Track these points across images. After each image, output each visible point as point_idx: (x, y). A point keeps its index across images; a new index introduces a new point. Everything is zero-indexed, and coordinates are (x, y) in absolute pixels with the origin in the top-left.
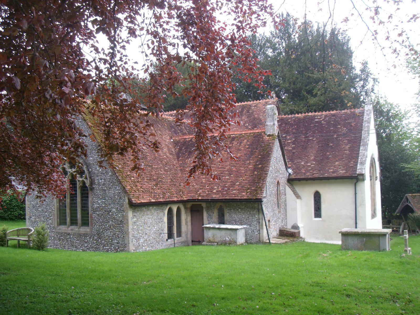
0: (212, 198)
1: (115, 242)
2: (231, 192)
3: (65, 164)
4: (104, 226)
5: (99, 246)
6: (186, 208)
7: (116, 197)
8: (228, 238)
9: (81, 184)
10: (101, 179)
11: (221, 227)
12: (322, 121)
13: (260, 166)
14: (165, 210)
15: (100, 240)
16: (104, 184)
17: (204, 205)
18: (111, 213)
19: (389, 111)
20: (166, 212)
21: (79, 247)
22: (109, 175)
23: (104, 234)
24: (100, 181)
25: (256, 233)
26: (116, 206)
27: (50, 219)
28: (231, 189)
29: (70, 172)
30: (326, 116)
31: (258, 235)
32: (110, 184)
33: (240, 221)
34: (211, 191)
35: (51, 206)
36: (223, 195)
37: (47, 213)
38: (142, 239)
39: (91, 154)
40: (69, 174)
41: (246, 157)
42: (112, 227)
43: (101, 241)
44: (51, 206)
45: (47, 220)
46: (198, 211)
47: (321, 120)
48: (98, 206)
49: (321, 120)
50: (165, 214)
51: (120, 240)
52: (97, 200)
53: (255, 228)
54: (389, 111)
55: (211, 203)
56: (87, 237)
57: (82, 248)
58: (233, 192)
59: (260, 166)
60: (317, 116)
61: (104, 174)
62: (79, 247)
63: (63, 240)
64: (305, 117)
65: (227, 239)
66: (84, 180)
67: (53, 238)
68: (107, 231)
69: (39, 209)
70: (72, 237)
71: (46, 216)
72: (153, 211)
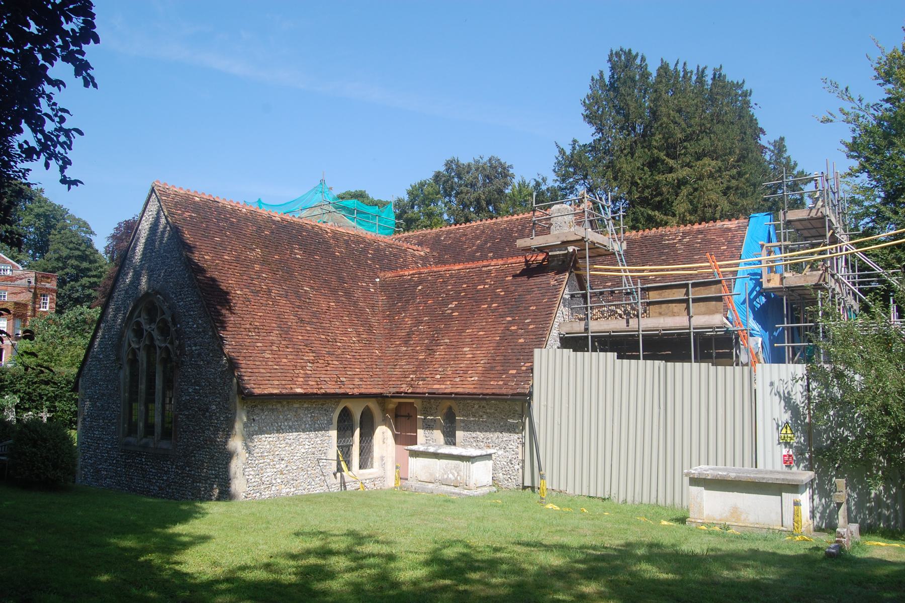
0: (431, 391)
1: (212, 474)
2: (469, 379)
3: (140, 317)
4: (196, 439)
5: (185, 480)
6: (384, 410)
7: (218, 380)
8: (453, 475)
9: (164, 355)
10: (195, 345)
11: (439, 451)
12: (676, 243)
13: (531, 327)
14: (333, 412)
15: (188, 469)
16: (199, 354)
17: (418, 404)
18: (208, 414)
19: (738, 83)
20: (335, 416)
21: (154, 481)
22: (207, 336)
23: (195, 456)
24: (194, 348)
25: (517, 467)
26: (218, 400)
27: (113, 424)
28: (469, 372)
29: (146, 331)
30: (685, 234)
31: (520, 471)
32: (209, 354)
33: (485, 440)
34: (433, 376)
35: (115, 398)
36: (454, 385)
37: (107, 412)
38: (268, 470)
39: (181, 295)
40: (145, 333)
41: (506, 310)
42: (208, 443)
43: (189, 471)
44: (115, 398)
45: (108, 425)
46: (409, 416)
47: (675, 241)
48: (188, 398)
49: (675, 241)
50: (331, 420)
51: (221, 470)
52: (186, 387)
53: (514, 457)
54: (738, 83)
55: (432, 400)
56: (168, 461)
57: (158, 484)
58: (473, 379)
59: (531, 327)
60: (819, 357)
61: (200, 333)
62: (154, 481)
63: (131, 465)
64: (644, 238)
65: (451, 476)
66: (168, 345)
67: (114, 462)
68: (199, 450)
69: (98, 404)
70: (143, 460)
71: (107, 416)
72: (301, 413)
